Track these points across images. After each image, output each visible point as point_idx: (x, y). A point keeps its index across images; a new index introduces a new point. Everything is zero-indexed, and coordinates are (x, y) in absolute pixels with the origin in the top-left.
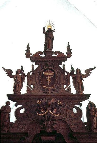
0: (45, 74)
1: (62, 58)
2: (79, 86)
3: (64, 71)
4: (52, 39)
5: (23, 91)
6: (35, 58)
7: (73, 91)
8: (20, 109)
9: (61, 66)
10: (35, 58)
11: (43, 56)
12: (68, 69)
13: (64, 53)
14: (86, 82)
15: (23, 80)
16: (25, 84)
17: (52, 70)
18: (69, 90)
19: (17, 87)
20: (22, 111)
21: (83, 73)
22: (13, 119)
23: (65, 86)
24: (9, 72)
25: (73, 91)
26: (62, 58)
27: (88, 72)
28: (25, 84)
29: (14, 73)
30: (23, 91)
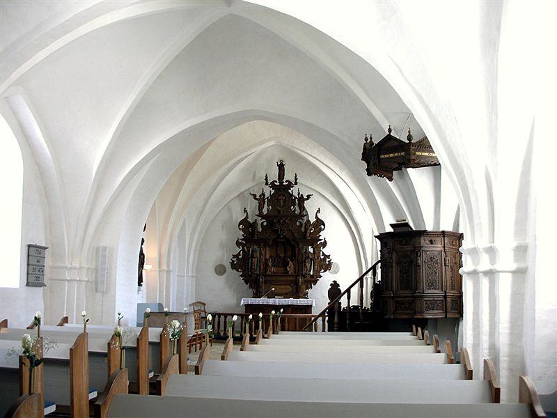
0: (279, 198)
1: (290, 185)
2: (302, 208)
3: (292, 195)
4: (517, 223)
5: (265, 211)
6: (273, 185)
7: (297, 212)
8: (263, 223)
9: (290, 191)
10: (273, 185)
11: (278, 184)
12: (296, 194)
13: (328, 267)
14: (306, 204)
15: (264, 203)
16: (266, 205)
17: (284, 195)
18: (295, 210)
19: (261, 208)
20: (265, 224)
21: (305, 197)
22: (260, 229)
23: (292, 207)
24: (254, 196)
25: (297, 212)
26: (290, 185)
27: (309, 197)
28: (266, 205)
29: (258, 197)
30: (265, 211)
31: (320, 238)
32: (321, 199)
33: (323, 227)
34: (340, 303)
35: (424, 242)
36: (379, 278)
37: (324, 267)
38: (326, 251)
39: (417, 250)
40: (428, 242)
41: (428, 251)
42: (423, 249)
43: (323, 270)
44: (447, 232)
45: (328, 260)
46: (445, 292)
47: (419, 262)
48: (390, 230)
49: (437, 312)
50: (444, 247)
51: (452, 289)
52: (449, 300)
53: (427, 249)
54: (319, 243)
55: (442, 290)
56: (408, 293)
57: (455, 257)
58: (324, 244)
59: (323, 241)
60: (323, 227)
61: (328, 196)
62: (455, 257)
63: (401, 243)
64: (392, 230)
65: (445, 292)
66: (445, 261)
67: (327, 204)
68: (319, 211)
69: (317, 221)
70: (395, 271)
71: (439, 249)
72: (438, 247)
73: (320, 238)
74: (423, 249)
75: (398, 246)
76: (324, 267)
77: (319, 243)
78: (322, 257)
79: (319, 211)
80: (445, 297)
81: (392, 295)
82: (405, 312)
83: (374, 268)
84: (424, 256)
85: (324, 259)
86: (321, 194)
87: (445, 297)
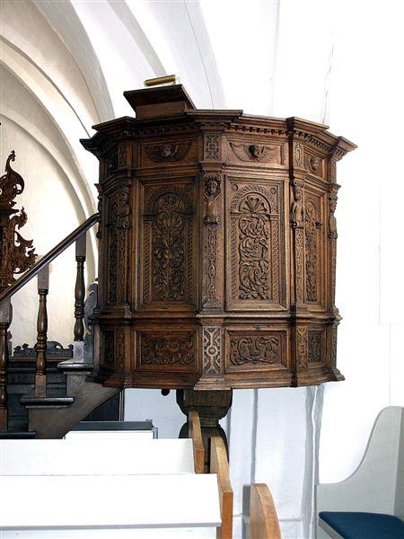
31: (14, 208)
32: (20, 137)
33: (19, 187)
34: (8, 336)
35: (229, 149)
36: (92, 273)
37: (21, 263)
38: (25, 232)
39: (203, 181)
40: (241, 152)
41: (241, 180)
42: (229, 172)
43: (18, 270)
44: (304, 124)
45: (28, 249)
46: (293, 309)
47: (215, 212)
48: (124, 110)
49: (266, 368)
50: (291, 171)
51: (311, 300)
52: (302, 331)
53: (237, 174)
54: (11, 217)
55: (282, 301)
56: (178, 310)
57: (317, 209)
58: (22, 220)
59: (18, 214)
60: (19, 187)
61: (33, 131)
62: (317, 209)
63: (158, 156)
64: (132, 114)
65: (293, 309)
66: (292, 210)
67: (30, 146)
68: (12, 157)
69: (8, 176)
70: (139, 241)
71: (276, 176)
72: (273, 168)
73: (14, 208)
74: (229, 172)
75: (151, 164)
76: (21, 263)
77: (11, 217)
78: (17, 245)
79: (12, 157)
80: (292, 322)
81: (128, 316)
82: (168, 367)
83: (78, 236)
84: (230, 195)
85: (22, 249)
86: (14, 123)
87: (292, 322)
